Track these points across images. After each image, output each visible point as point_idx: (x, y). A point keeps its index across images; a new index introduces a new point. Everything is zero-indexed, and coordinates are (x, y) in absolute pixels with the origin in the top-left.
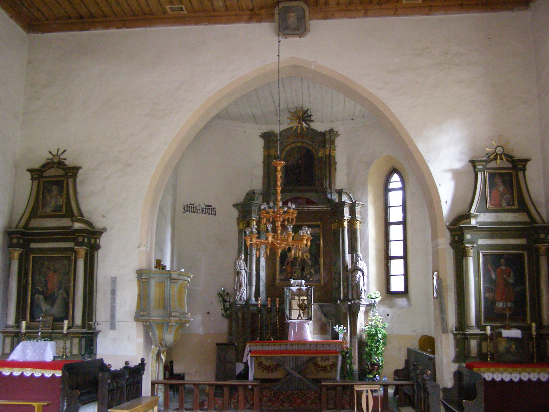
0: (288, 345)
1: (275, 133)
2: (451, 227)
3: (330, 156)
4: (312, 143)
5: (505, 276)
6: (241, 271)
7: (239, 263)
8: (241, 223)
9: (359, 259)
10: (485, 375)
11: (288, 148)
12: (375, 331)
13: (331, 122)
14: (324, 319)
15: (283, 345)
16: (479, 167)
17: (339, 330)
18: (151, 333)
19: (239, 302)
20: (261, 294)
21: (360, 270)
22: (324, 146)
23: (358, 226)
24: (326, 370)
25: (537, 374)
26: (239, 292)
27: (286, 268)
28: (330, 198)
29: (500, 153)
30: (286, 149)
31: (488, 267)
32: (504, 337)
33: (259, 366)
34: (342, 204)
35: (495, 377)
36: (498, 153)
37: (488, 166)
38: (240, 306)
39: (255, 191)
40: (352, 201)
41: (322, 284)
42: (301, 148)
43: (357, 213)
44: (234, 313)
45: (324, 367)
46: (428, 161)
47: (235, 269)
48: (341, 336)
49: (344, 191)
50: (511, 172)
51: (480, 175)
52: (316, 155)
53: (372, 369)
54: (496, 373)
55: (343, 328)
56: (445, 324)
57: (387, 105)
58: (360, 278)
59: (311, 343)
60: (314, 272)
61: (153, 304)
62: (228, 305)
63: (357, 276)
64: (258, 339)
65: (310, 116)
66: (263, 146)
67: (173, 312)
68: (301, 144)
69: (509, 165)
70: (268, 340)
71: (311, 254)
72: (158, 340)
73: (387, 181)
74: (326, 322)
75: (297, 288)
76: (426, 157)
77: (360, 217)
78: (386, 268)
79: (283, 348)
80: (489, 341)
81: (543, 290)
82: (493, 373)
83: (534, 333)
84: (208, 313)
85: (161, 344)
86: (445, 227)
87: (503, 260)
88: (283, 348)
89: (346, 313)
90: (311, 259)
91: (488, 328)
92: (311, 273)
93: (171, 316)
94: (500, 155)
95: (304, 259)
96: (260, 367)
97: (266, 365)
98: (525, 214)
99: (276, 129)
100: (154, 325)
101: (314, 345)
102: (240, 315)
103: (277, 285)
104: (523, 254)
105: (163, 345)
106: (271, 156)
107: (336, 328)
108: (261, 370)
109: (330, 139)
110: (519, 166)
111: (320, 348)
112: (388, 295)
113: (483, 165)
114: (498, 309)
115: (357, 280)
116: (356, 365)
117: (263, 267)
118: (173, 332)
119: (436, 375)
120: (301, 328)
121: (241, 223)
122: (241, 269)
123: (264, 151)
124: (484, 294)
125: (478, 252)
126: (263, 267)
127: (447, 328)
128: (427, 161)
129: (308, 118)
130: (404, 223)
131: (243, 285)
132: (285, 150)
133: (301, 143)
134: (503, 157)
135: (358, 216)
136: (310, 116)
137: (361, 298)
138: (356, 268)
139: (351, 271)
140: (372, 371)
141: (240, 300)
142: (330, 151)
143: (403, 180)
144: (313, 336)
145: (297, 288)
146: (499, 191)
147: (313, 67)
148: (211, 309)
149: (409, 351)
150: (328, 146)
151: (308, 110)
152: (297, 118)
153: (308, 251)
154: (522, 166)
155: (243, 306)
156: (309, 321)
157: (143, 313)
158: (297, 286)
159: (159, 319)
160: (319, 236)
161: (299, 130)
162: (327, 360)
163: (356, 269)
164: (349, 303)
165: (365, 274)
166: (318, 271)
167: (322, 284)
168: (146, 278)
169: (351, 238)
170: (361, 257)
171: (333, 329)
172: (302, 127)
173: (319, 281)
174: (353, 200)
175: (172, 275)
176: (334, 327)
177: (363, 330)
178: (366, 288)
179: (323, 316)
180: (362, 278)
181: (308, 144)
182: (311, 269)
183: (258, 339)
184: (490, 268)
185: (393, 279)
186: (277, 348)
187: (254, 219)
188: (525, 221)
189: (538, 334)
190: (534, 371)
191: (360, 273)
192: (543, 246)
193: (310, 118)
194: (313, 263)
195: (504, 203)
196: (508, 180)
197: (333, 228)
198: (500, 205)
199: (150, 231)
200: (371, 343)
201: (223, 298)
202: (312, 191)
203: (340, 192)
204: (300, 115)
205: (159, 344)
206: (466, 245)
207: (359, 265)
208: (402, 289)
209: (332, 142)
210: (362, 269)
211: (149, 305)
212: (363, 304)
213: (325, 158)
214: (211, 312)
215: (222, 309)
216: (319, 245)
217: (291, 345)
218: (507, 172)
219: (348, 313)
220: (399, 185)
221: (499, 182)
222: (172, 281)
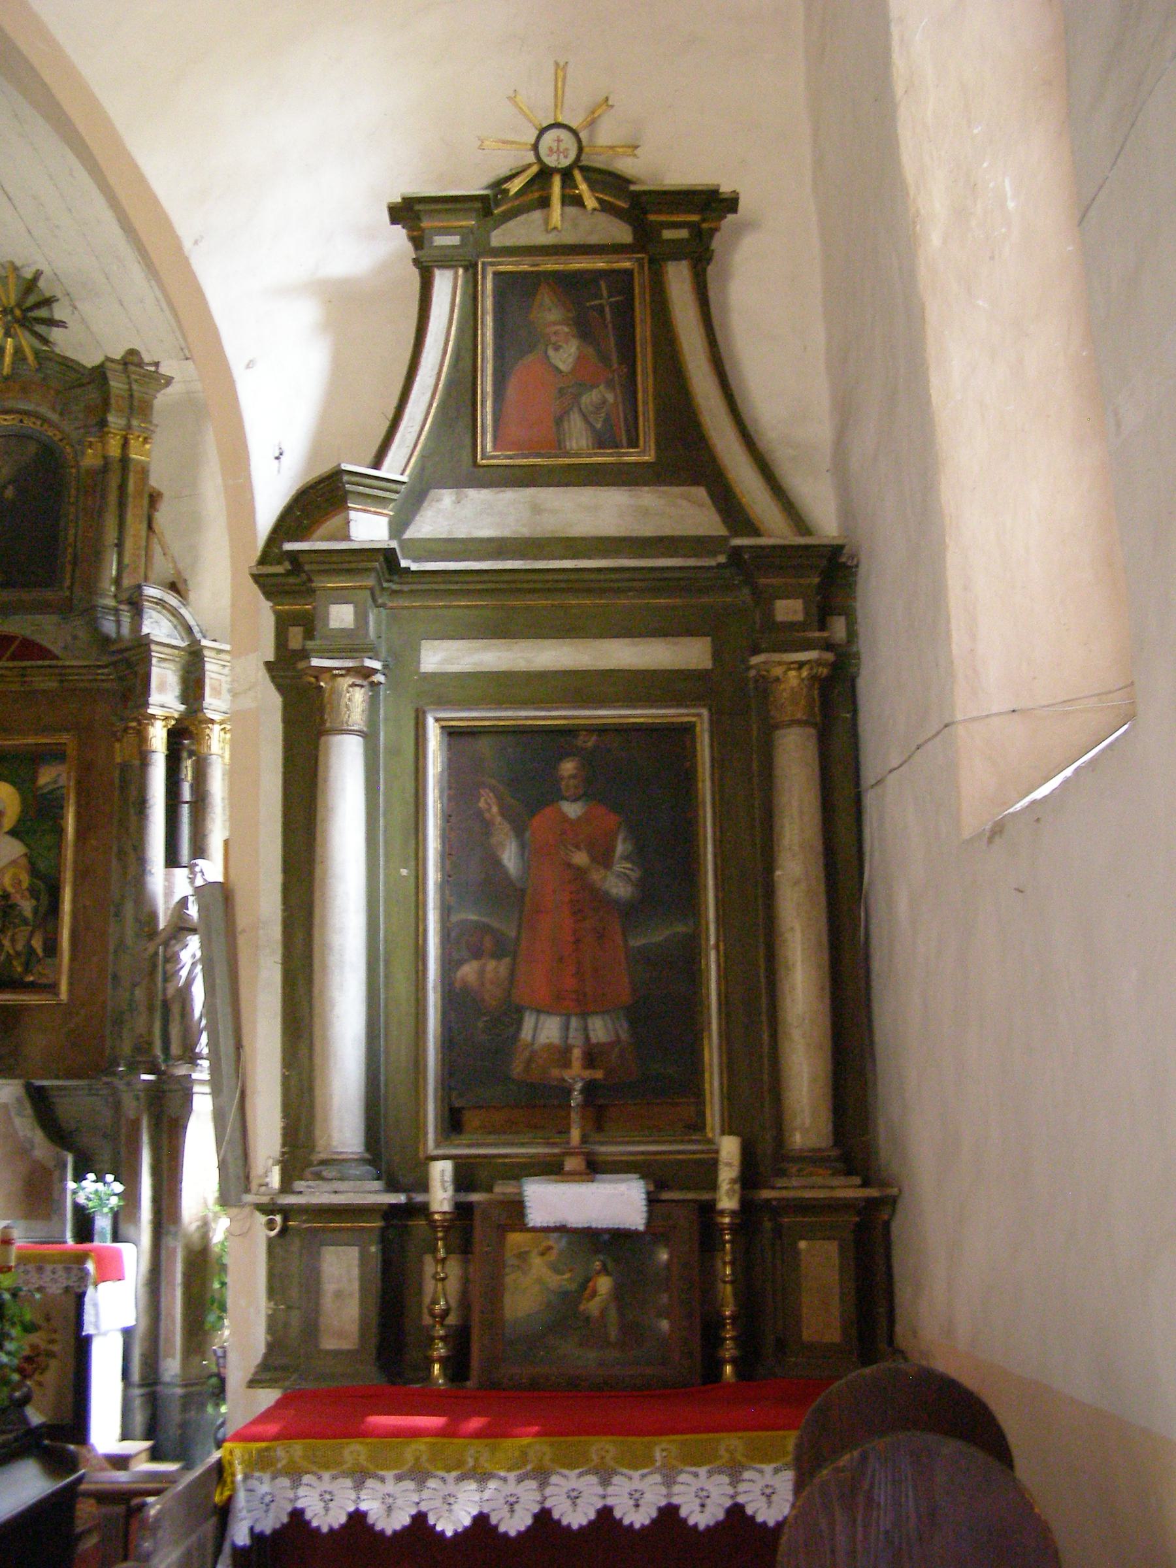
3: (125, 460)
4: (61, 414)
5: (581, 858)
10: (301, 1491)
16: (440, 241)
25: (657, 1478)
28: (114, 635)
29: (565, 163)
31: (482, 804)
32: (534, 1230)
35: (371, 1506)
36: (551, 161)
37: (498, 238)
42: (21, 437)
43: (213, 689)
46: (196, 242)
50: (627, 265)
51: (444, 284)
54: (382, 1480)
60: (44, 950)
65: (48, 302)
69: (622, 233)
71: (34, 871)
74: (51, 1164)
80: (442, 1253)
81: (788, 935)
82: (360, 1477)
83: (727, 1202)
87: (568, 767)
89: (135, 1126)
91: (441, 1172)
92: (31, 951)
94: (567, 175)
98: (701, 492)
104: (687, 730)
109: (131, 396)
110: (667, 234)
113: (465, 233)
114: (529, 1062)
116: (173, 1356)
124: (448, 965)
125: (417, 718)
128: (187, 244)
129: (42, 313)
133: (19, 417)
134: (583, 187)
136: (48, 302)
146: (557, 368)
150: (115, 421)
151: (38, 275)
153: (24, 861)
154: (683, 234)
167: (64, 996)
181: (45, 420)
184: (495, 809)
188: (701, 532)
189: (748, 1209)
190: (639, 1461)
192: (789, 666)
193: (51, 310)
194: (42, 910)
195: (578, 437)
196: (607, 309)
198: (558, 446)
202: (44, 607)
204: (8, 298)
206: (315, 662)
209: (139, 408)
218: (601, 265)
221: (554, 324)
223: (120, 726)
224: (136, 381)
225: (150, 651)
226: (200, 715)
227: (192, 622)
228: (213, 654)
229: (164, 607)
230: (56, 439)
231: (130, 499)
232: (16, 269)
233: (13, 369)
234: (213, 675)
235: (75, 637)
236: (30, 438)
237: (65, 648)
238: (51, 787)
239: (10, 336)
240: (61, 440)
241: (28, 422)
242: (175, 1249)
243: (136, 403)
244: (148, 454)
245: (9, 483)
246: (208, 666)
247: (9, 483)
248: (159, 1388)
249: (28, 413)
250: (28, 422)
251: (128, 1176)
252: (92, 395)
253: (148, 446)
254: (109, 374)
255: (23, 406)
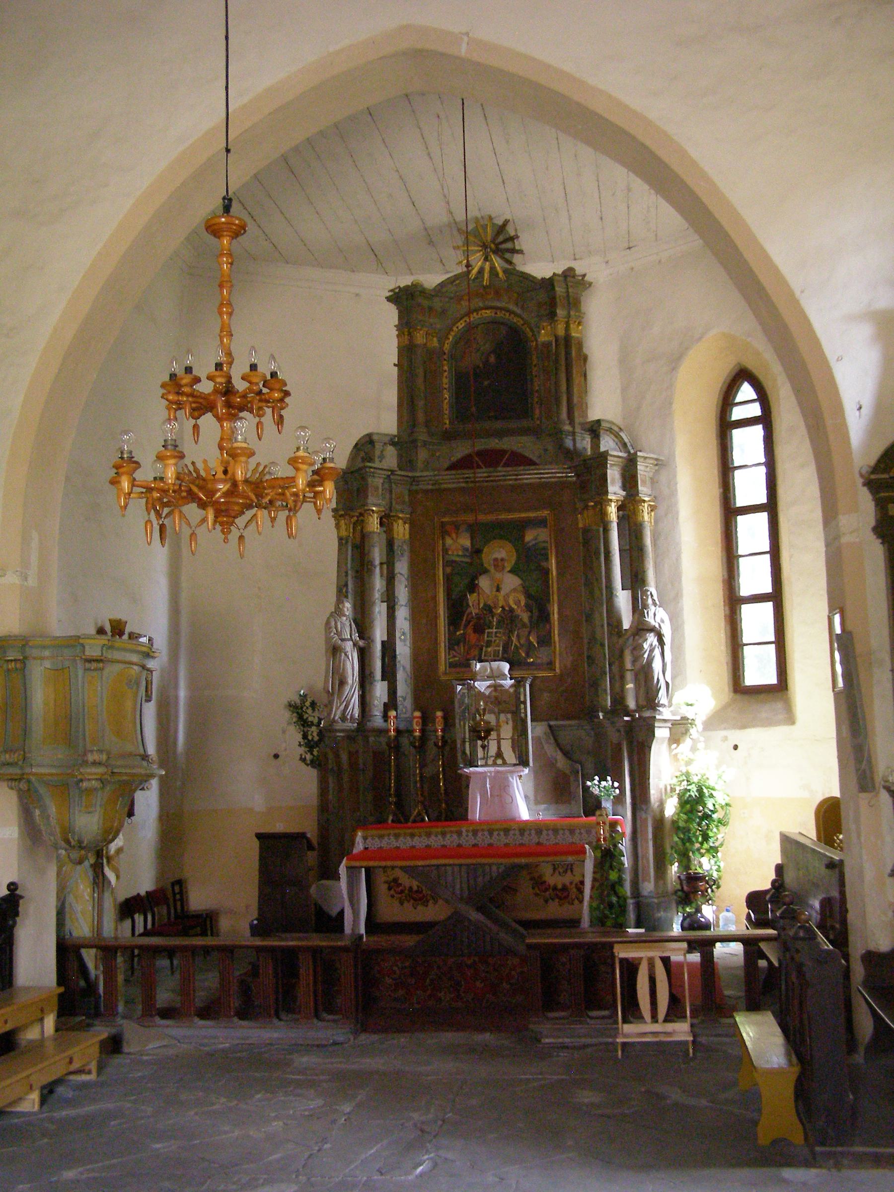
0: (464, 834)
1: (424, 289)
2: (873, 477)
3: (568, 339)
6: (343, 644)
7: (336, 623)
8: (342, 522)
9: (650, 601)
11: (461, 325)
12: (697, 791)
13: (575, 259)
14: (562, 762)
15: (452, 832)
17: (600, 791)
18: (37, 812)
19: (340, 726)
20: (399, 703)
21: (652, 630)
22: (552, 315)
23: (646, 517)
24: (566, 897)
26: (339, 697)
27: (464, 634)
28: (572, 448)
30: (455, 329)
33: (390, 889)
34: (601, 459)
38: (342, 734)
39: (375, 438)
40: (629, 452)
41: (558, 670)
43: (643, 481)
44: (331, 756)
45: (561, 890)
47: (328, 639)
48: (607, 805)
49: (603, 424)
52: (533, 339)
53: (689, 892)
55: (613, 783)
56: (864, 763)
57: (675, 138)
58: (652, 651)
59: (524, 828)
60: (538, 643)
61: (38, 729)
62: (315, 734)
63: (646, 646)
64: (391, 818)
65: (512, 239)
66: (397, 323)
67: (92, 751)
68: (493, 315)
70: (414, 821)
71: (528, 596)
72: (58, 830)
73: (727, 401)
74: (567, 772)
75: (488, 683)
76: (795, 281)
77: (650, 493)
78: (728, 628)
79: (451, 840)
84: (276, 756)
85: (68, 842)
86: (860, 481)
88: (467, 841)
90: (528, 608)
92: (530, 643)
93: (85, 763)
95: (512, 610)
96: (392, 892)
97: (411, 888)
99: (431, 280)
100: (42, 790)
101: (533, 832)
102: (344, 757)
103: (443, 678)
105: (73, 843)
106: (417, 346)
107: (597, 786)
108: (397, 903)
109: (568, 296)
111: (548, 840)
112: (738, 696)
115: (646, 656)
116: (649, 882)
117: (404, 634)
118: (98, 808)
119: (847, 911)
120: (502, 788)
121: (342, 522)
122: (343, 640)
123: (398, 336)
126: (404, 634)
127: (872, 772)
128: (797, 293)
129: (508, 245)
130: (771, 507)
131: (350, 681)
132: (451, 330)
133: (494, 311)
135: (644, 490)
136: (512, 239)
137: (659, 705)
138: (641, 627)
139: (630, 633)
140: (692, 896)
141: (343, 718)
142: (567, 328)
143: (763, 398)
144: (533, 807)
145: (488, 683)
147: (463, 51)
148: (284, 745)
149: (787, 842)
150: (561, 312)
151: (506, 222)
152: (479, 246)
153: (521, 588)
155: (351, 737)
156: (520, 768)
157: (7, 756)
158: (489, 678)
159: (53, 771)
160: (545, 548)
161: (486, 276)
162: (569, 872)
163: (641, 628)
164: (626, 718)
165: (667, 639)
166: (545, 641)
167: (558, 670)
168: (15, 660)
169: (630, 550)
170: (655, 597)
171: (586, 789)
172: (493, 268)
173: (550, 665)
174: (630, 448)
175: (87, 648)
176: (589, 783)
177: (666, 789)
178: (669, 680)
179: (559, 756)
180: (657, 652)
181: (511, 312)
182: (530, 633)
183: (391, 818)
185: (749, 654)
186: (436, 841)
187: (374, 509)
191: (652, 639)
194: (535, 618)
197: (581, 525)
199: (35, 535)
200: (686, 821)
201: (300, 717)
202: (525, 432)
203: (595, 429)
204: (486, 237)
205: (63, 843)
207: (650, 619)
208: (772, 679)
209: (574, 303)
210: (657, 626)
211: (26, 731)
212: (665, 721)
213: (556, 345)
214: (282, 754)
215: (300, 745)
216: (546, 572)
217: (470, 834)
219: (625, 743)
220: (755, 410)
222: (88, 665)
223: (579, 505)
224: (571, 286)
225: (607, 459)
226: (637, 498)
227: (626, 440)
228: (642, 460)
229: (611, 432)
230: (519, 324)
231: (574, 362)
232: (490, 218)
233: (490, 281)
234: (642, 473)
235: (546, 450)
236: (502, 324)
237: (540, 457)
238: (534, 542)
239: (487, 261)
240: (522, 325)
241: (500, 314)
242: (646, 819)
243: (571, 299)
244: (581, 332)
245: (491, 353)
246: (639, 467)
247: (491, 353)
248: (641, 899)
249: (501, 309)
250: (500, 314)
251: (618, 777)
252: (542, 296)
253: (580, 328)
254: (556, 284)
255: (498, 304)
